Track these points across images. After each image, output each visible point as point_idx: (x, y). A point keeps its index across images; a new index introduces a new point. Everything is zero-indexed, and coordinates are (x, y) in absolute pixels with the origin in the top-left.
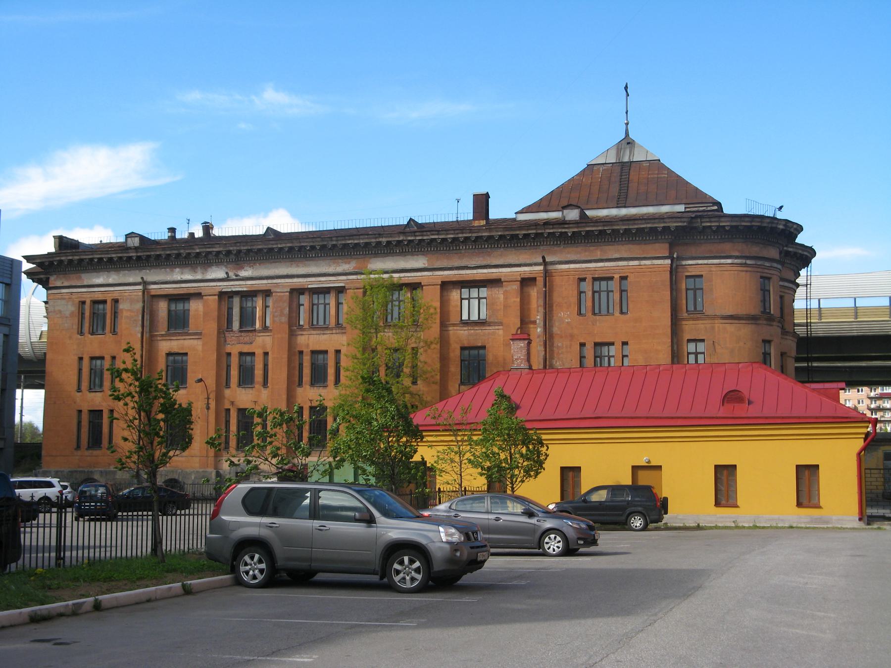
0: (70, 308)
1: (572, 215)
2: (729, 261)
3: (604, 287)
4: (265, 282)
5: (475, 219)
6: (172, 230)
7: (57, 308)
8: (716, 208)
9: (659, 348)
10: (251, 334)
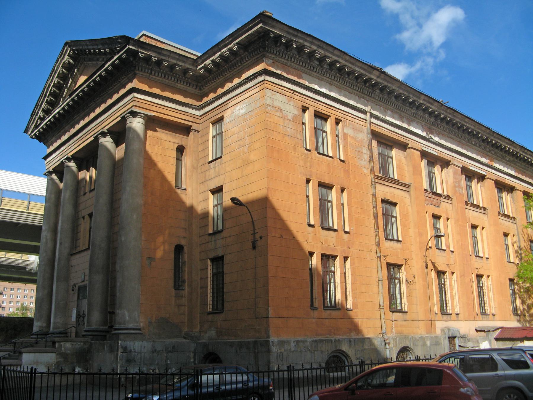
7: (276, 104)
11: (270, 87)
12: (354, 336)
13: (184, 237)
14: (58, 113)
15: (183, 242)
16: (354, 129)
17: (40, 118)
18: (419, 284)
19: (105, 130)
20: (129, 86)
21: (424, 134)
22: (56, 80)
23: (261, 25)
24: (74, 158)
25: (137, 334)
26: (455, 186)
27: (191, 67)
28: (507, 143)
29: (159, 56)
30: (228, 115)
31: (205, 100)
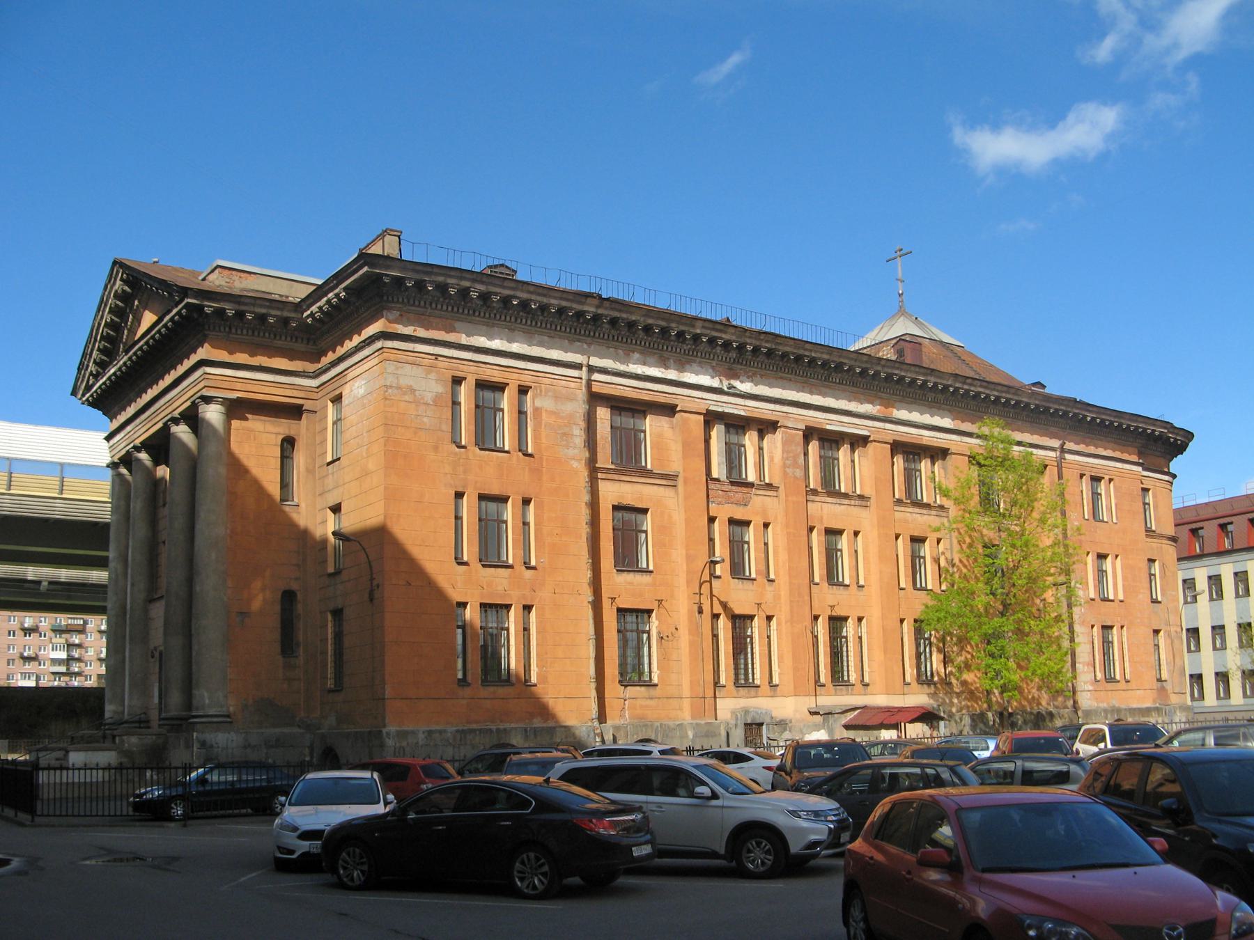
7: (404, 382)
11: (392, 357)
12: (537, 723)
13: (297, 579)
14: (114, 374)
15: (294, 586)
16: (557, 397)
17: (91, 374)
18: (684, 638)
19: (176, 414)
20: (194, 359)
21: (715, 383)
22: (107, 317)
23: (366, 269)
24: (145, 446)
25: (226, 721)
26: (785, 466)
27: (293, 315)
28: (918, 373)
29: (237, 307)
30: (346, 391)
31: (325, 360)
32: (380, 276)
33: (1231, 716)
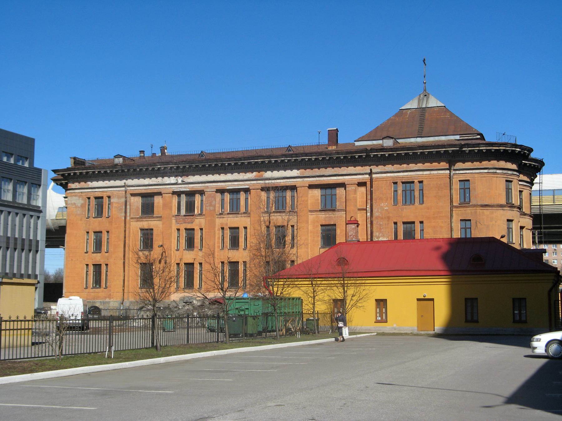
0: (79, 202)
1: (388, 143)
2: (486, 171)
3: (408, 188)
4: (200, 185)
5: (329, 145)
6: (142, 152)
7: (73, 202)
8: (479, 137)
9: (442, 225)
10: (192, 217)
32: (88, 172)
33: (251, 340)
